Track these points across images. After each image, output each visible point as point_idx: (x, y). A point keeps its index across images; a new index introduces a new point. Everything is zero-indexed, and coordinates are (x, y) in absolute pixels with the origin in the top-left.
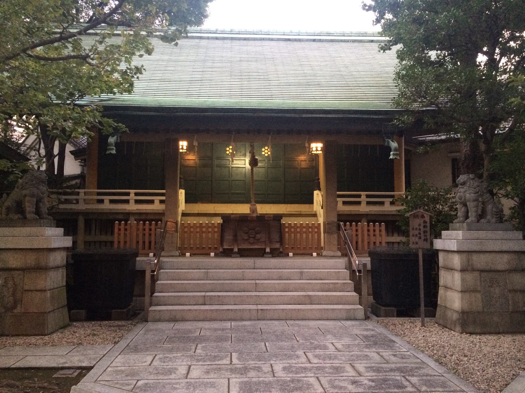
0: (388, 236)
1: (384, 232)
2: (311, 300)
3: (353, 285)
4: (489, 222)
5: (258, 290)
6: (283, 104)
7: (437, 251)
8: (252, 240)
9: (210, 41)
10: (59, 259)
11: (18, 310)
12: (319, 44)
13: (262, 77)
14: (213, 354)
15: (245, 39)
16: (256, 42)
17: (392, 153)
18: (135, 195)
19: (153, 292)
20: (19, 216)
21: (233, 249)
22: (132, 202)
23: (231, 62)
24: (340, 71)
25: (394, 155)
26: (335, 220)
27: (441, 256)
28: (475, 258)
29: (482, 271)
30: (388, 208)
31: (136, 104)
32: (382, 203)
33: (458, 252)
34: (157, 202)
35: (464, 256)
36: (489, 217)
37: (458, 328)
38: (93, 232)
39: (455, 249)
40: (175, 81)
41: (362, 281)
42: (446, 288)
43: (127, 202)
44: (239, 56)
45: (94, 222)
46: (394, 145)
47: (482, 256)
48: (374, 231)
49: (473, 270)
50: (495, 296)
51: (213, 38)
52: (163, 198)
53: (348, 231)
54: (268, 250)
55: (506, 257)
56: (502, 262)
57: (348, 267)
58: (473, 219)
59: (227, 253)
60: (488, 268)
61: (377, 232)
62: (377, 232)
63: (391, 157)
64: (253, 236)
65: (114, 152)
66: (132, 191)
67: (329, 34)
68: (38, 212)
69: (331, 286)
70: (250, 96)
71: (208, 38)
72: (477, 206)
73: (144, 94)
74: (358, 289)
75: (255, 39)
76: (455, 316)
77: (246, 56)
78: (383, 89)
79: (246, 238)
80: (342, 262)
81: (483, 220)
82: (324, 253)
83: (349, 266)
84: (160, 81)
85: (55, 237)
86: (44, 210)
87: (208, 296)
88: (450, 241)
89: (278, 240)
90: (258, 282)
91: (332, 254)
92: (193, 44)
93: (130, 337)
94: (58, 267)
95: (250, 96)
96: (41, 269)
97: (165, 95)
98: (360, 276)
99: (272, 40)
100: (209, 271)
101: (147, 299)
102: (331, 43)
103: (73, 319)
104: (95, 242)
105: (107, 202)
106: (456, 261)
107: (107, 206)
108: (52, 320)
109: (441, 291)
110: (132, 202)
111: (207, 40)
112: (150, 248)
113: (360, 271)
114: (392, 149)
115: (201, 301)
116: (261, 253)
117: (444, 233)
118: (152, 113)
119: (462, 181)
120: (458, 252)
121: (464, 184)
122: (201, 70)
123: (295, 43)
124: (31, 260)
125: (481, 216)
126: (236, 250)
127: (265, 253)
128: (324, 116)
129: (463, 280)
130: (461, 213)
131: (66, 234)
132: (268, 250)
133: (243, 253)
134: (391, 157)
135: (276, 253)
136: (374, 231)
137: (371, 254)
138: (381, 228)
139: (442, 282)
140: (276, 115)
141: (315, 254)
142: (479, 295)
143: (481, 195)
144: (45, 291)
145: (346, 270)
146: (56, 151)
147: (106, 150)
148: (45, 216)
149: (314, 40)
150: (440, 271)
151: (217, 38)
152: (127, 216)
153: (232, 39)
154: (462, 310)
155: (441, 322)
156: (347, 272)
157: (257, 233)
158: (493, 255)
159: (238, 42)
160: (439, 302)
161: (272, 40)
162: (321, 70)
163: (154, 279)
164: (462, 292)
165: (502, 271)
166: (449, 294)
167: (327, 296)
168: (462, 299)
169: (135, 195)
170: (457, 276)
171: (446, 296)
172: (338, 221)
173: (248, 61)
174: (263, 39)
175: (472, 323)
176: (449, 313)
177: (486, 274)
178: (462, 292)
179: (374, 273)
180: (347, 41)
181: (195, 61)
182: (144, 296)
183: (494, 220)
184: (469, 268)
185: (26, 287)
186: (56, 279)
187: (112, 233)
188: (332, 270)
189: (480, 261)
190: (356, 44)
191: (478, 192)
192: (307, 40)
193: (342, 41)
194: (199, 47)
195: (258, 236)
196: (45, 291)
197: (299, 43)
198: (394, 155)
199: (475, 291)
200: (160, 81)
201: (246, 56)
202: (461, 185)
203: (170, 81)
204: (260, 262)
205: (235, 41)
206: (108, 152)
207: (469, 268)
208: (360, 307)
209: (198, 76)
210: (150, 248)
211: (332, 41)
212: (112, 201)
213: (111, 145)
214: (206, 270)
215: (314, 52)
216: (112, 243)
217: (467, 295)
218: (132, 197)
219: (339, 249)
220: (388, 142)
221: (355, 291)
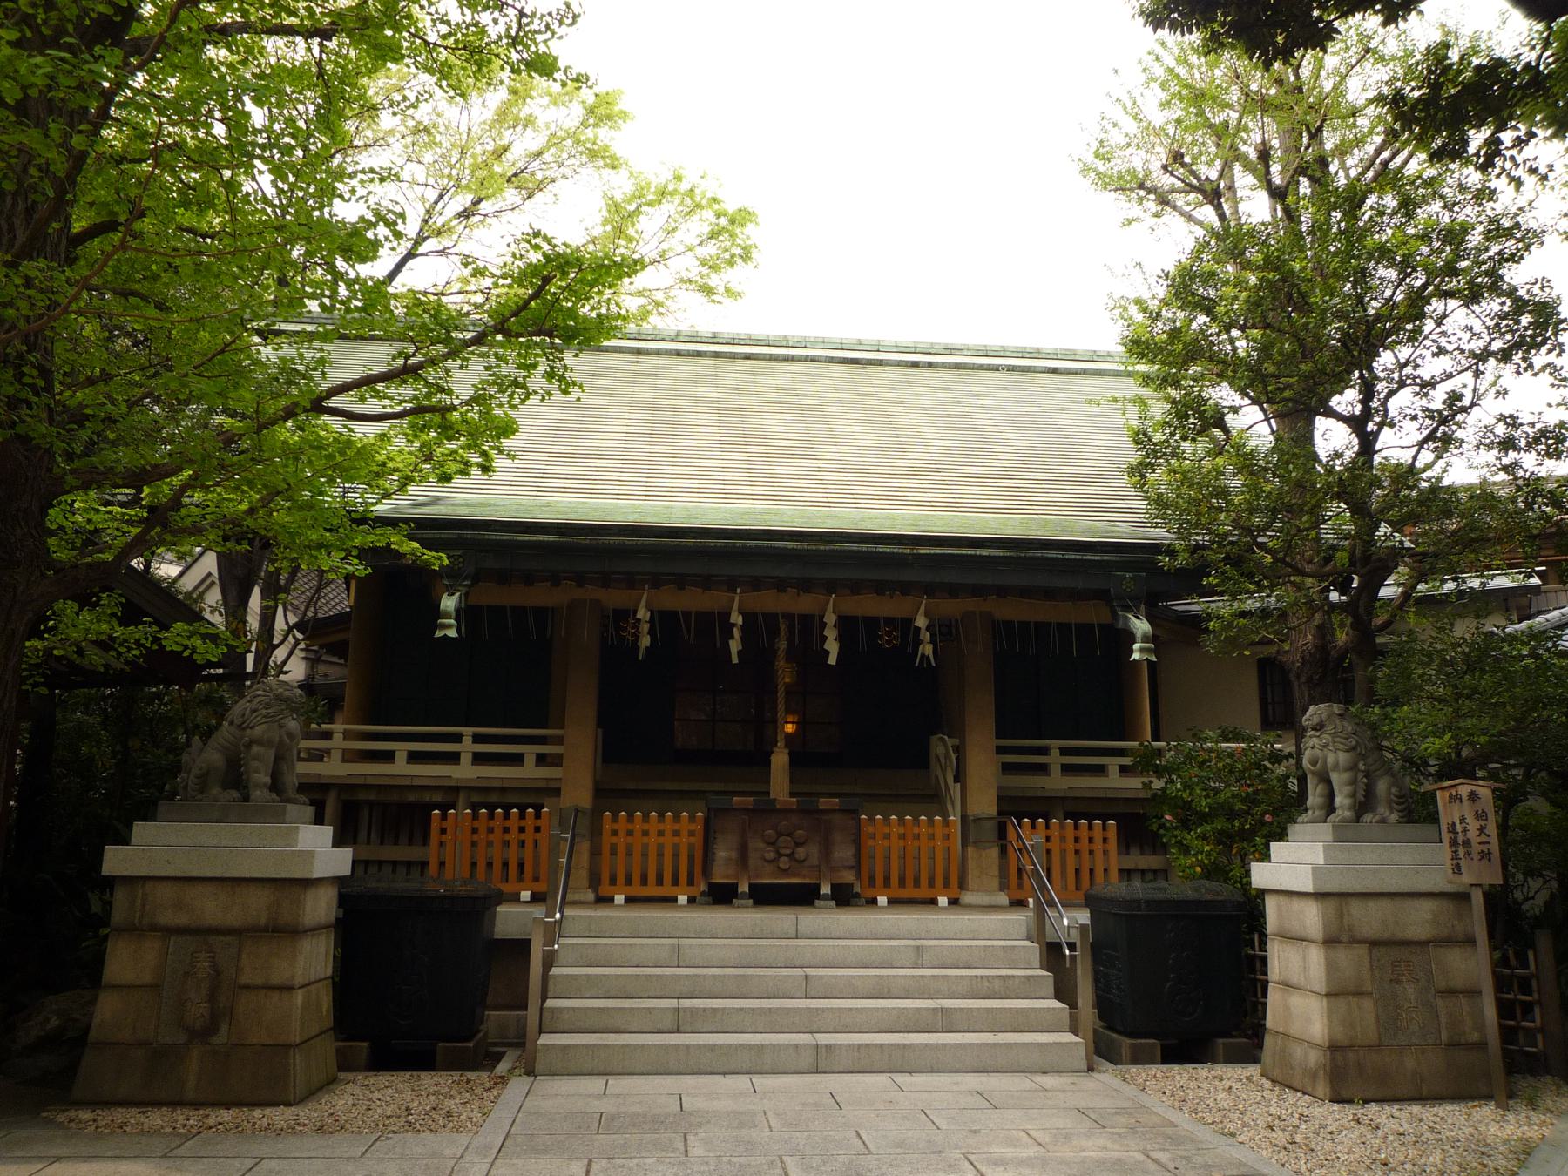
0: (1128, 853)
1: (1113, 844)
2: (949, 1021)
3: (1051, 982)
4: (1383, 821)
5: (813, 993)
6: (863, 519)
7: (1262, 893)
8: (784, 863)
9: (662, 359)
10: (321, 907)
11: (221, 1038)
12: (927, 372)
13: (798, 451)
14: (735, 1160)
15: (748, 357)
16: (774, 363)
17: (1136, 646)
18: (474, 742)
19: (544, 998)
20: (235, 794)
21: (735, 886)
22: (466, 759)
23: (719, 412)
24: (985, 440)
25: (1142, 650)
26: (993, 811)
27: (1271, 906)
28: (1356, 909)
29: (1373, 944)
30: (1115, 783)
31: (463, 513)
32: (517, 759)
33: (1318, 896)
34: (1114, 771)
35: (1332, 904)
36: (1382, 810)
37: (1322, 1088)
38: (363, 835)
39: (1310, 888)
40: (586, 456)
41: (1079, 972)
42: (1287, 985)
43: (1043, 769)
44: (736, 397)
45: (366, 812)
46: (1141, 626)
47: (1372, 904)
48: (1091, 840)
49: (1355, 941)
50: (1407, 1005)
51: (669, 353)
52: (1127, 761)
53: (1029, 836)
54: (825, 889)
55: (1426, 908)
56: (1419, 921)
57: (1034, 934)
58: (1348, 814)
59: (722, 896)
60: (1386, 936)
61: (1098, 845)
62: (1098, 845)
63: (1136, 656)
64: (788, 852)
65: (452, 633)
66: (1055, 744)
67: (950, 351)
68: (276, 786)
69: (998, 985)
70: (774, 498)
71: (658, 353)
72: (1353, 782)
73: (511, 489)
74: (1064, 992)
75: (773, 358)
76: (1314, 1058)
77: (753, 397)
78: (1095, 486)
79: (771, 855)
80: (1019, 920)
81: (1368, 817)
82: (967, 898)
83: (1038, 931)
84: (550, 455)
85: (320, 851)
86: (291, 781)
87: (685, 1009)
88: (1291, 866)
89: (852, 862)
90: (809, 971)
91: (984, 899)
92: (621, 365)
93: (502, 1115)
94: (316, 929)
95: (774, 498)
96: (285, 932)
97: (564, 491)
98: (1073, 958)
99: (813, 360)
100: (684, 942)
101: (532, 1013)
102: (956, 372)
103: (346, 1064)
104: (380, 863)
105: (401, 757)
106: (1311, 918)
107: (401, 768)
108: (300, 1067)
109: (1274, 997)
110: (1056, 770)
111: (655, 358)
112: (613, 881)
113: (1072, 946)
114: (1139, 635)
115: (668, 1022)
116: (804, 897)
117: (1274, 846)
118: (552, 538)
119: (1316, 720)
120: (1318, 896)
121: (1319, 727)
122: (647, 430)
123: (870, 369)
124: (255, 906)
125: (1363, 806)
126: (744, 888)
127: (818, 896)
128: (970, 552)
129: (1331, 967)
130: (1314, 798)
131: (338, 842)
132: (825, 889)
133: (765, 897)
134: (1136, 656)
135: (844, 898)
136: (1091, 840)
137: (1090, 902)
138: (1078, 833)
139: (1275, 970)
140: (855, 547)
141: (943, 901)
142: (1368, 1004)
143: (1363, 757)
144: (290, 988)
145: (1028, 943)
146: (253, 622)
147: (436, 627)
148: (292, 793)
149: (915, 364)
150: (1269, 946)
151: (678, 353)
152: (451, 794)
153: (717, 355)
154: (1330, 1041)
155: (1276, 1074)
156: (1033, 950)
157: (798, 845)
158: (1398, 902)
159: (730, 362)
160: (1269, 1023)
161: (813, 360)
162: (941, 438)
163: (549, 961)
164: (1328, 995)
165: (1426, 943)
166: (1297, 1001)
167: (988, 1010)
168: (1330, 1012)
169: (474, 742)
170: (1316, 956)
171: (1287, 1008)
172: (1000, 813)
173: (760, 410)
174: (792, 358)
175: (1352, 1076)
176: (1298, 1052)
177: (1383, 949)
178: (1328, 995)
179: (1099, 946)
180: (996, 368)
181: (630, 408)
182: (525, 1008)
183: (1394, 817)
184: (1345, 938)
185: (244, 979)
186: (314, 960)
187: (425, 841)
188: (995, 943)
189: (1370, 919)
190: (1017, 376)
191: (1353, 749)
192: (899, 364)
193: (981, 367)
194: (635, 374)
195: (801, 852)
196: (290, 988)
197: (879, 369)
198: (1142, 650)
199: (1359, 993)
200: (550, 455)
201: (753, 397)
202: (1314, 729)
203: (572, 456)
204: (809, 918)
205: (721, 361)
206: (439, 634)
207: (1345, 938)
208: (1069, 1038)
209: (639, 445)
210: (675, 882)
211: (958, 366)
212: (414, 757)
213: (447, 615)
214: (675, 941)
215: (999, 400)
216: (424, 864)
217: (1342, 1003)
218: (1055, 760)
219: (1003, 887)
220: (1127, 619)
221: (1059, 995)
